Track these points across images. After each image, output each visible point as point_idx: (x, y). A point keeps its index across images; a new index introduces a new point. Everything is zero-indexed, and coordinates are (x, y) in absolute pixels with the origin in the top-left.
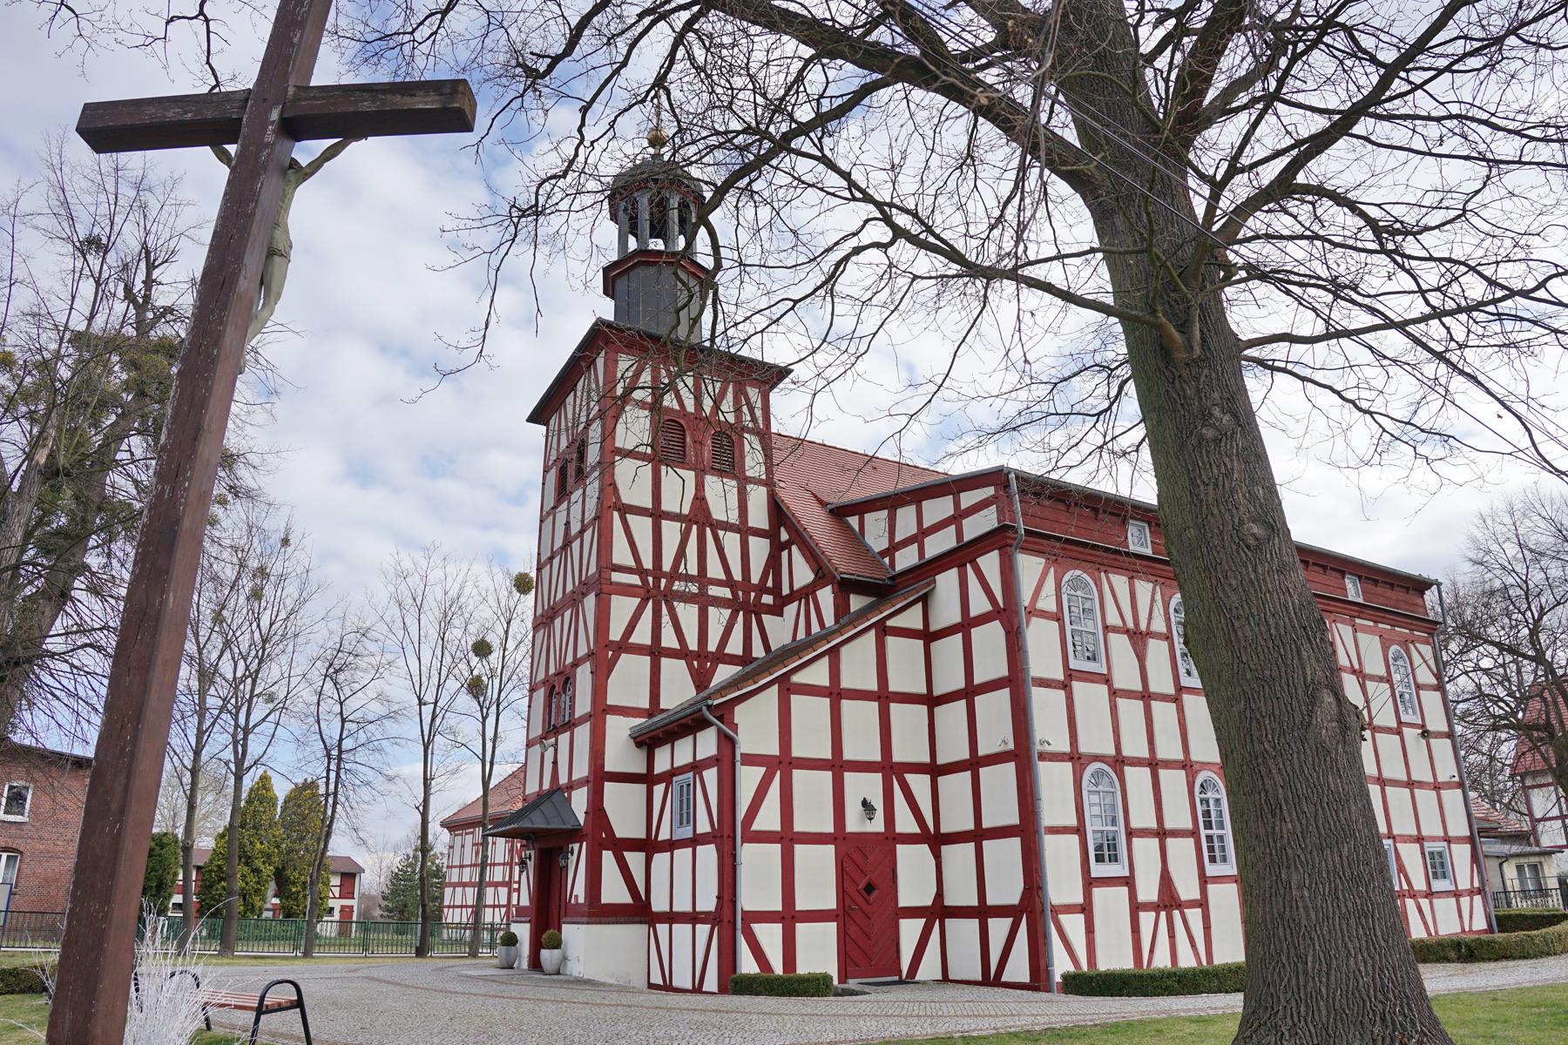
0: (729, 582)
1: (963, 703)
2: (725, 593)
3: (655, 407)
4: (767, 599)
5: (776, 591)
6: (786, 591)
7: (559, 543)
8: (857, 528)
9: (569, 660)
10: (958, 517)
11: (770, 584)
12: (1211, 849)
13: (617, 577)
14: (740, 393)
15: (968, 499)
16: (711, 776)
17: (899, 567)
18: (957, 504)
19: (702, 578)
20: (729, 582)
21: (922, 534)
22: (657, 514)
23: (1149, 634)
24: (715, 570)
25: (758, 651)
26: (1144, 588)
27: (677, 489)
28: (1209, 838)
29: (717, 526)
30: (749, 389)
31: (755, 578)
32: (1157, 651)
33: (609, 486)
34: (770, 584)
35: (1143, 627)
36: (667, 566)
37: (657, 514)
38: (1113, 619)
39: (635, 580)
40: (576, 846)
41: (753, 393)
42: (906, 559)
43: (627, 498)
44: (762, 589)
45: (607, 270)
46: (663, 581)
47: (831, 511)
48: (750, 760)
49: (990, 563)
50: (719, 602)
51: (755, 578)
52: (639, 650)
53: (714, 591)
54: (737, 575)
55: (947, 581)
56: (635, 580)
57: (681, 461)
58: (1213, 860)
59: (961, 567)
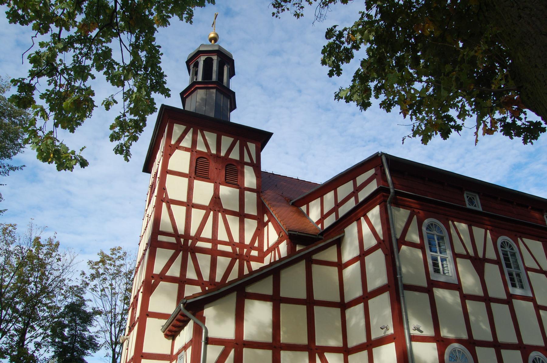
0: (231, 243)
1: (237, 210)
2: (229, 249)
3: (192, 149)
4: (254, 253)
5: (260, 248)
8: (305, 211)
11: (256, 244)
12: (512, 279)
13: (161, 238)
15: (361, 180)
17: (325, 227)
18: (355, 184)
19: (214, 240)
20: (231, 243)
21: (338, 205)
22: (189, 205)
23: (485, 260)
24: (222, 236)
26: (479, 232)
27: (204, 191)
28: (510, 274)
29: (226, 212)
30: (249, 144)
31: (247, 241)
32: (491, 270)
34: (256, 244)
35: (481, 255)
36: (193, 232)
37: (189, 205)
38: (459, 249)
39: (173, 240)
41: (252, 147)
42: (328, 222)
43: (172, 195)
44: (251, 247)
45: (180, 94)
46: (190, 241)
47: (293, 204)
49: (374, 213)
50: (224, 254)
51: (247, 241)
52: (172, 280)
53: (220, 247)
54: (236, 239)
55: (352, 230)
56: (173, 240)
57: (205, 178)
58: (514, 285)
59: (358, 220)
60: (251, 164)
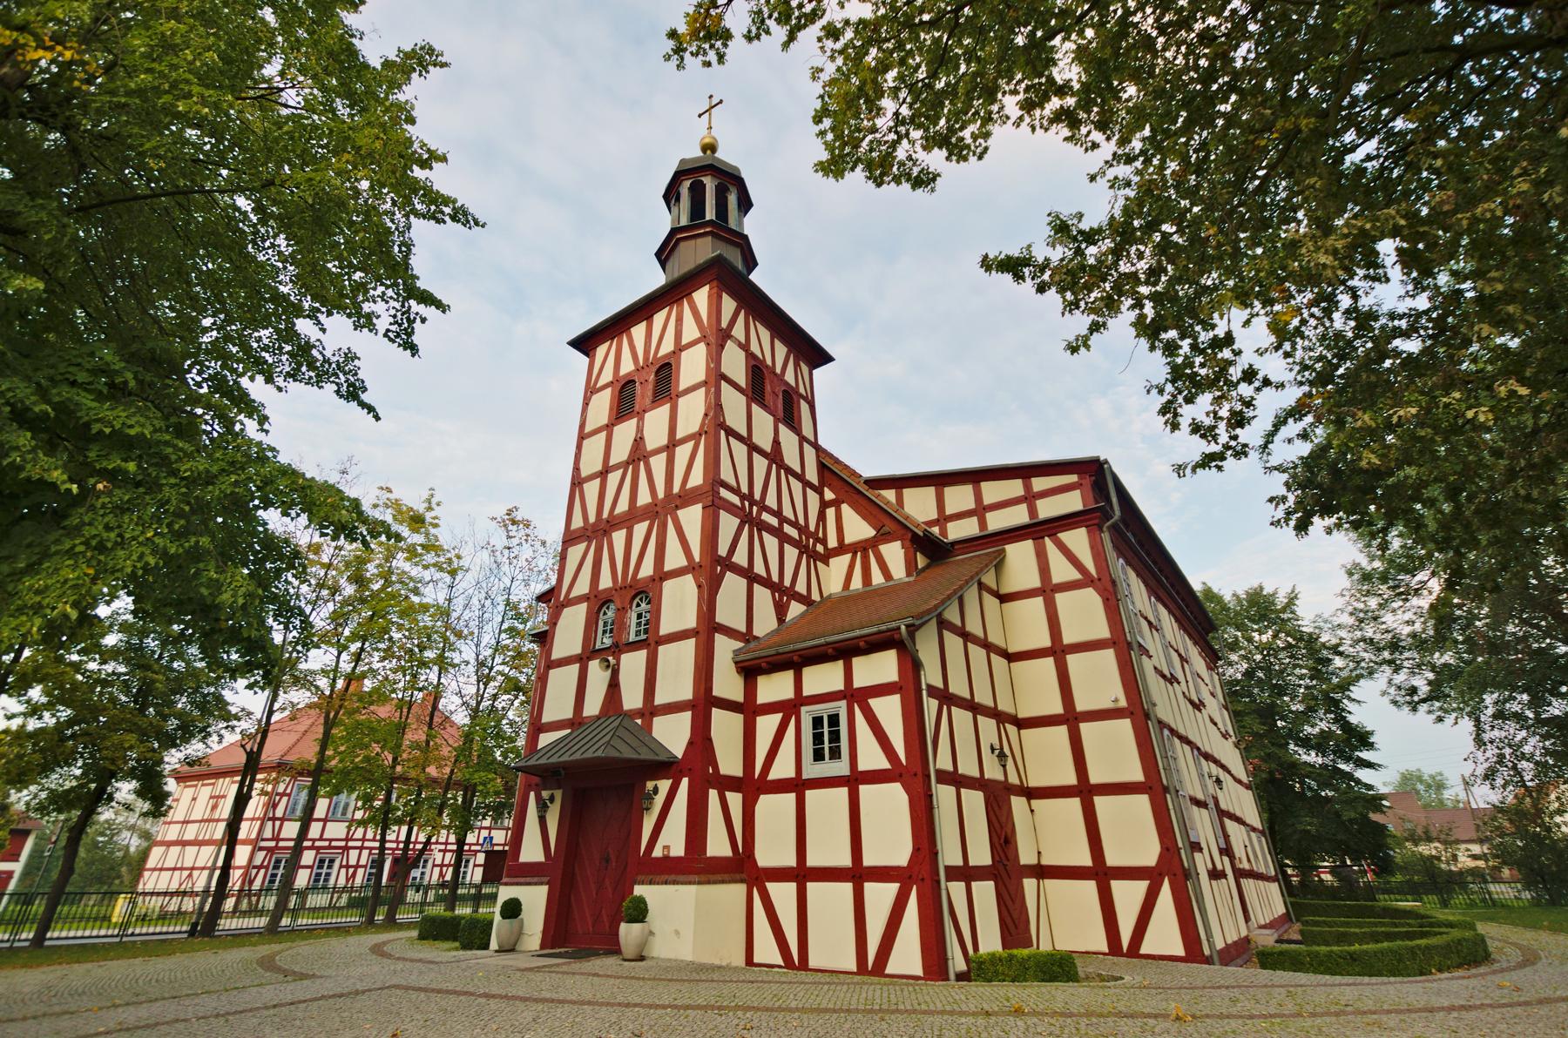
6: (832, 542)
7: (620, 453)
9: (647, 570)
14: (797, 365)
15: (1039, 484)
16: (889, 710)
19: (778, 514)
31: (812, 528)
40: (664, 785)
56: (735, 500)
60: (806, 399)
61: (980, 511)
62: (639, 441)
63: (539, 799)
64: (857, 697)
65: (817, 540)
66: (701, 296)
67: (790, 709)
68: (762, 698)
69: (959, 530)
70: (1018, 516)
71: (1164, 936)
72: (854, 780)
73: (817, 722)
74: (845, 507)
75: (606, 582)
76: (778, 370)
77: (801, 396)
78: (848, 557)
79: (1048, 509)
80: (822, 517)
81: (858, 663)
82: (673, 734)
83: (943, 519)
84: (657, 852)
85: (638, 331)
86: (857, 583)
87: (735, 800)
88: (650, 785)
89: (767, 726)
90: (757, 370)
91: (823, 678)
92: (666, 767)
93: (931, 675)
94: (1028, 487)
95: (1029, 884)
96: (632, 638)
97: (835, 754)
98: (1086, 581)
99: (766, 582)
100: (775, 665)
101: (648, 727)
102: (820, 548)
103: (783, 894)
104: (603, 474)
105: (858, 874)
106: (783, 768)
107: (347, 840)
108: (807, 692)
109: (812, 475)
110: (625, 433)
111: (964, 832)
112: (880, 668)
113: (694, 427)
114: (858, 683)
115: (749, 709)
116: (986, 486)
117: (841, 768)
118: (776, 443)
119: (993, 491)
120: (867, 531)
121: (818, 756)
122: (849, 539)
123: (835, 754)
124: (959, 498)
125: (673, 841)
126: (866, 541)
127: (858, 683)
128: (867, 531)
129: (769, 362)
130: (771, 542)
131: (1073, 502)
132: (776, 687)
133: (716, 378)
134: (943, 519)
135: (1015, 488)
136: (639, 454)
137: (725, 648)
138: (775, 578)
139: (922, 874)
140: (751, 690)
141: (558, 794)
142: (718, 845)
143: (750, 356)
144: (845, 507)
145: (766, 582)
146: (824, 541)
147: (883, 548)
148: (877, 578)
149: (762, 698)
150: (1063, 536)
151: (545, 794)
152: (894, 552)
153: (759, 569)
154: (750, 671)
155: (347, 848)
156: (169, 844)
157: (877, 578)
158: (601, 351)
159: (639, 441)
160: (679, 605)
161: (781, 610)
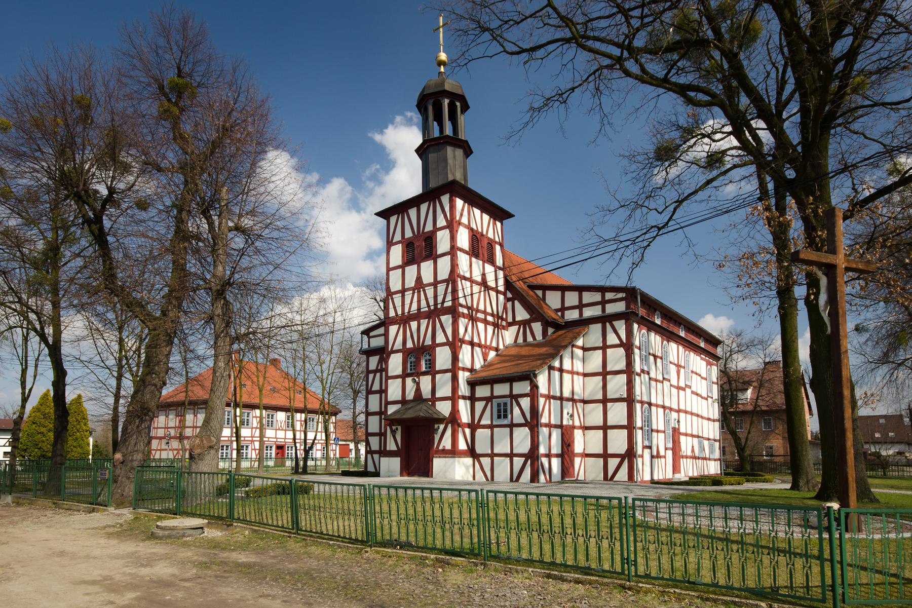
0: (492, 315)
7: (411, 282)
10: (603, 303)
14: (495, 224)
15: (609, 296)
19: (485, 312)
25: (501, 347)
33: (454, 266)
40: (442, 427)
48: (542, 396)
61: (581, 306)
62: (419, 279)
63: (391, 429)
64: (515, 398)
65: (502, 319)
66: (445, 199)
67: (488, 400)
68: (478, 395)
69: (572, 315)
70: (596, 311)
71: (623, 475)
72: (512, 426)
73: (499, 405)
74: (516, 302)
75: (409, 345)
76: (485, 233)
77: (496, 242)
78: (516, 327)
79: (611, 309)
80: (505, 308)
81: (515, 384)
82: (444, 408)
83: (563, 309)
84: (441, 448)
85: (413, 212)
86: (520, 340)
87: (467, 431)
88: (436, 426)
89: (479, 406)
90: (476, 237)
91: (502, 389)
92: (441, 420)
93: (543, 389)
94: (603, 296)
95: (577, 460)
96: (424, 369)
97: (505, 417)
98: (621, 345)
99: (480, 345)
100: (483, 382)
101: (434, 405)
102: (504, 323)
103: (486, 461)
104: (403, 292)
105: (511, 456)
106: (486, 421)
107: (252, 437)
108: (495, 394)
109: (501, 288)
110: (411, 271)
111: (550, 442)
112: (522, 387)
113: (446, 276)
114: (515, 392)
115: (472, 399)
116: (585, 294)
117: (506, 422)
118: (484, 275)
119: (588, 297)
120: (527, 316)
121: (499, 417)
122: (518, 318)
123: (505, 417)
124: (572, 298)
125: (447, 443)
126: (526, 320)
127: (515, 392)
128: (527, 316)
129: (480, 230)
130: (481, 326)
131: (620, 307)
132: (483, 391)
133: (453, 251)
134: (563, 309)
135: (597, 297)
136: (419, 285)
137: (463, 376)
138: (483, 343)
139: (532, 455)
140: (473, 391)
141: (399, 428)
142: (462, 446)
143: (471, 230)
144: (516, 302)
145: (480, 345)
146: (506, 320)
147: (533, 325)
148: (530, 339)
149: (478, 395)
150: (615, 323)
151: (394, 428)
152: (537, 327)
153: (476, 340)
154: (472, 384)
155: (252, 441)
156: (160, 438)
157: (530, 339)
158: (393, 219)
159: (419, 279)
160: (443, 357)
161: (485, 356)
